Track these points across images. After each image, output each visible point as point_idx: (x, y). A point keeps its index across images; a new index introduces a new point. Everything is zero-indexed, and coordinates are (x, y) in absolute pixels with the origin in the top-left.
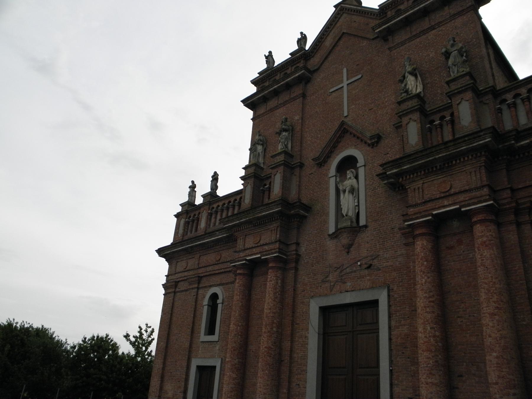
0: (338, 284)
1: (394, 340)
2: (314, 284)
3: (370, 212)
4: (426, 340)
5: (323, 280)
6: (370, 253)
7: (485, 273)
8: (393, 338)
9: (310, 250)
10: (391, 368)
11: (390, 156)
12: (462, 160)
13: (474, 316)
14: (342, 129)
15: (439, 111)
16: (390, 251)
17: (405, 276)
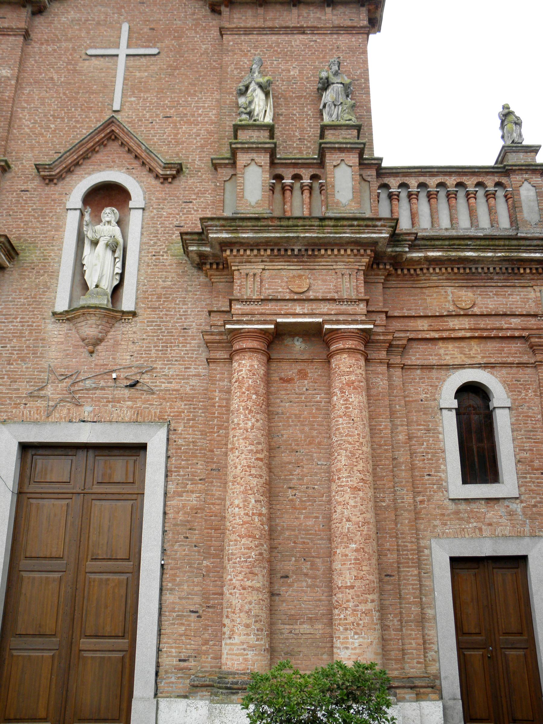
0: (64, 406)
1: (170, 516)
2: (10, 398)
3: (143, 291)
4: (246, 519)
5: (31, 393)
6: (137, 361)
7: (349, 428)
8: (169, 512)
9: (6, 333)
10: (163, 562)
11: (193, 208)
12: (336, 252)
13: (314, 488)
14: (108, 131)
15: (295, 165)
16: (175, 365)
17: (200, 411)
